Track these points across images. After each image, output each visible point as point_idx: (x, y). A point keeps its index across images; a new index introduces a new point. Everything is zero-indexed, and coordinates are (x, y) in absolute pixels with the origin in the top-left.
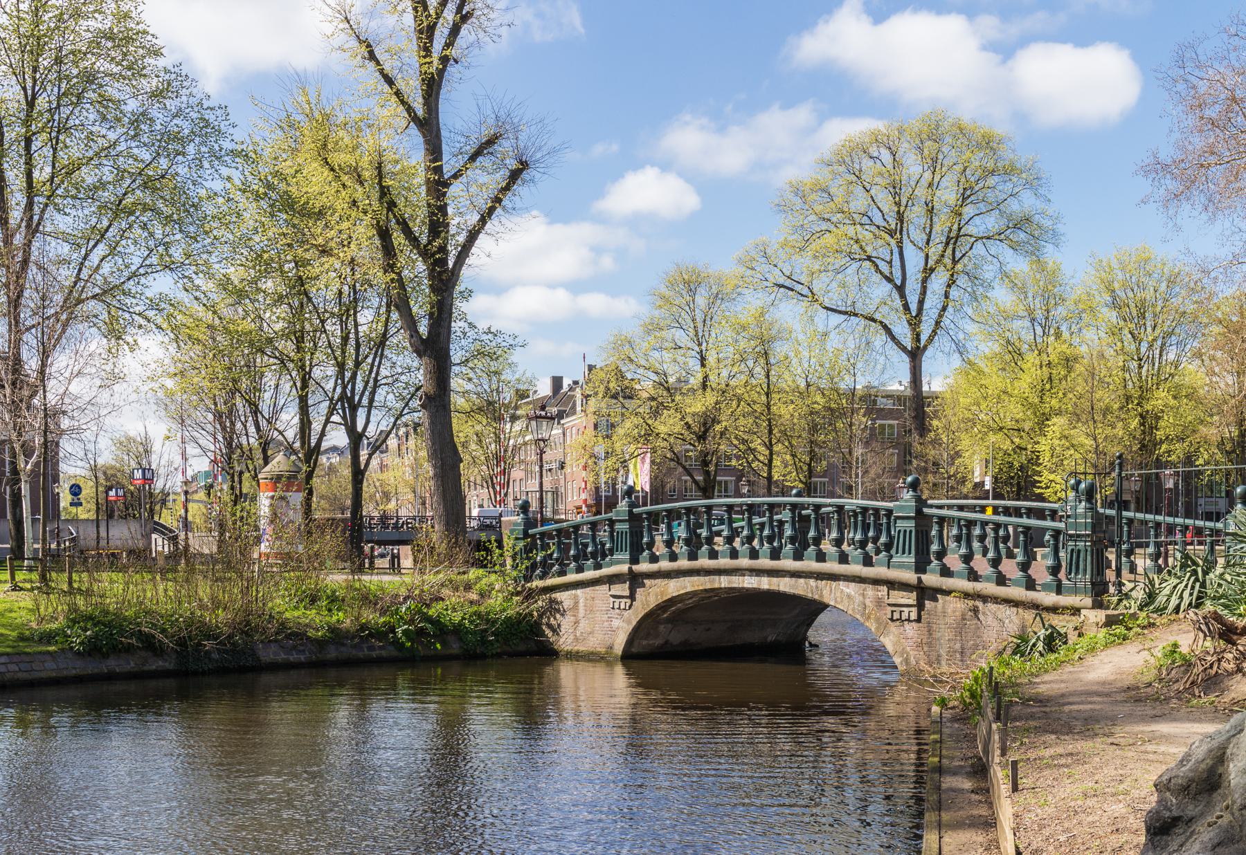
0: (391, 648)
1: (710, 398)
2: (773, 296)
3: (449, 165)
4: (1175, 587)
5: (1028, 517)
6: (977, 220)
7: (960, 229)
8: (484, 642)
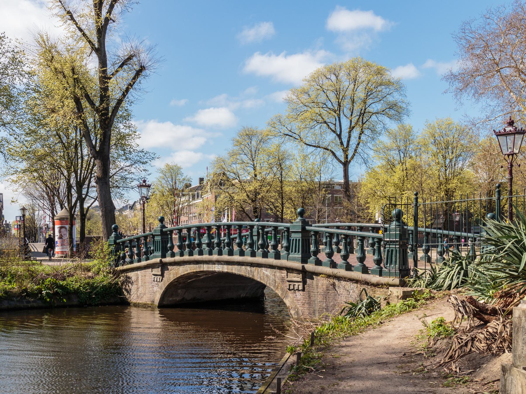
0: (40, 302)
1: (257, 185)
2: (283, 139)
3: (110, 69)
4: (448, 273)
5: (373, 232)
6: (373, 105)
7: (365, 109)
8: (90, 298)
